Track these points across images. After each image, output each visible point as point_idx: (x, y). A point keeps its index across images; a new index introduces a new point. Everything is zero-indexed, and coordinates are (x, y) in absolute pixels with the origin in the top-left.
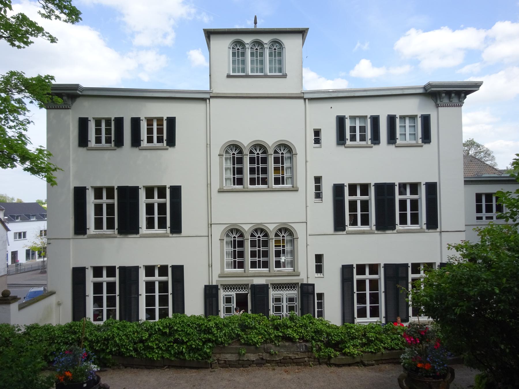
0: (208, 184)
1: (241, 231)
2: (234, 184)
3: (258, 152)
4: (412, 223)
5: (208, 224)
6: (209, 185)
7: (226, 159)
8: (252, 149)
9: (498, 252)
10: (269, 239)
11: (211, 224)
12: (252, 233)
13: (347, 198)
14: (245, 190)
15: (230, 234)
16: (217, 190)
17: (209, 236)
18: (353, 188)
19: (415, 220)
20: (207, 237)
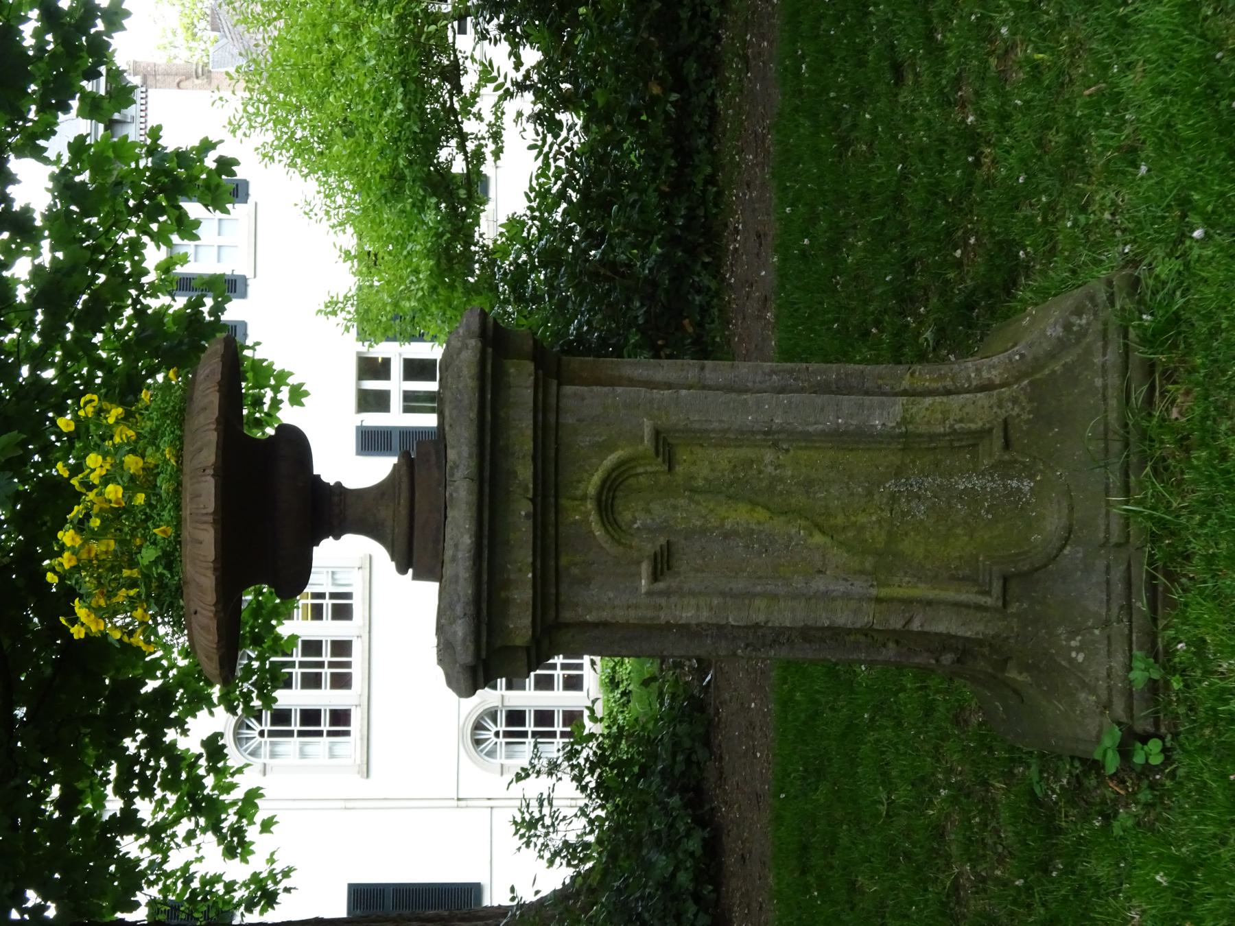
0: (346, 808)
1: (481, 717)
2: (347, 733)
3: (256, 733)
5: (458, 807)
6: (349, 803)
7: (273, 755)
8: (246, 750)
9: (576, 862)
10: (503, 706)
11: (459, 799)
12: (486, 754)
14: (368, 566)
15: (487, 746)
18: (372, 401)
20: (494, 810)
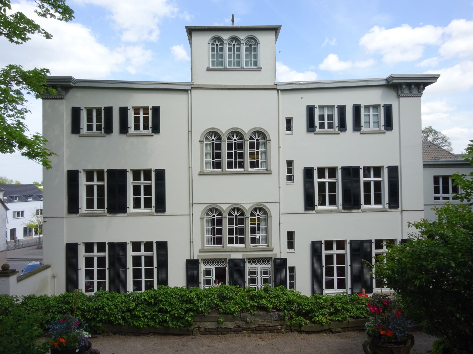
0: (189, 168)
1: (219, 211)
2: (213, 168)
3: (235, 138)
4: (376, 203)
5: (190, 204)
6: (190, 169)
7: (206, 145)
8: (230, 135)
10: (246, 218)
11: (192, 204)
12: (230, 212)
13: (317, 180)
14: (223, 173)
15: (210, 213)
16: (197, 173)
17: (191, 215)
18: (321, 172)
19: (378, 200)
20: (189, 216)
